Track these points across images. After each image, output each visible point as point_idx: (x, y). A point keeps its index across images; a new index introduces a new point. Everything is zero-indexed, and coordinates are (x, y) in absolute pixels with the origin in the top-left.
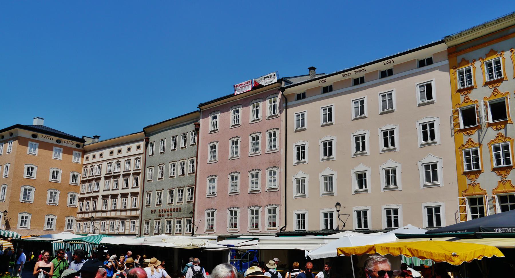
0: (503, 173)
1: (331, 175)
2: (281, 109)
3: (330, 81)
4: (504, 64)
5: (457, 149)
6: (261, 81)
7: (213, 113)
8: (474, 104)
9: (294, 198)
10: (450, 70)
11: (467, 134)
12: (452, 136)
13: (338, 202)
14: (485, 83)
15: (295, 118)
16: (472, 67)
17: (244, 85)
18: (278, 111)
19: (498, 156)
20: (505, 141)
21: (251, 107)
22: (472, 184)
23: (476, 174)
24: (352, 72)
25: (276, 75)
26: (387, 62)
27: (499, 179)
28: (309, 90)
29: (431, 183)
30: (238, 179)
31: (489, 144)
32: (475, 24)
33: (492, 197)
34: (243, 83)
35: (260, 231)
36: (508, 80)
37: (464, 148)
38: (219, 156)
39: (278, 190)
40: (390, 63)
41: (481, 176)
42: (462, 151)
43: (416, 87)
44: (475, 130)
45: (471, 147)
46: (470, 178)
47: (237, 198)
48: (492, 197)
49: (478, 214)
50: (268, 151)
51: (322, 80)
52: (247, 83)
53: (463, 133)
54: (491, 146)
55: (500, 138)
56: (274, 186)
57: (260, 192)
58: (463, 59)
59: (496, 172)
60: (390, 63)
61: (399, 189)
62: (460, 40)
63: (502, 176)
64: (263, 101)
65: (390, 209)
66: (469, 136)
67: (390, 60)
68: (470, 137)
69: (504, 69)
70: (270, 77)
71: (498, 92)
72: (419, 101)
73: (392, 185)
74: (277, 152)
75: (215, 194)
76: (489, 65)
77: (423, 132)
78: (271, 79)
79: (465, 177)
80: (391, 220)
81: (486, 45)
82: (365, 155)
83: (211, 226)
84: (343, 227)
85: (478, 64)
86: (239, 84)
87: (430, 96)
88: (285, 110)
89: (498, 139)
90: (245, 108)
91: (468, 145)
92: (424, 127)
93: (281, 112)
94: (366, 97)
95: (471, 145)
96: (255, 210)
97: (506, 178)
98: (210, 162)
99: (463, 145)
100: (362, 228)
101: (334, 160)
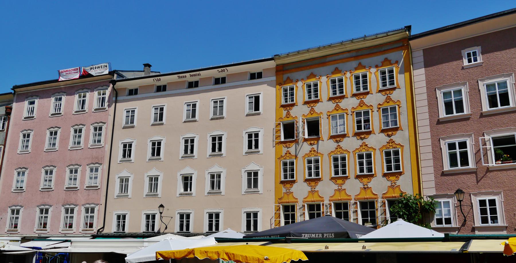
0: (313, 184)
2: (110, 103)
3: (164, 80)
4: (320, 87)
5: (277, 159)
7: (30, 98)
9: (115, 197)
11: (286, 146)
12: (273, 147)
13: (162, 204)
15: (125, 114)
16: (295, 86)
17: (70, 72)
18: (106, 104)
20: (368, 150)
21: (77, 96)
22: (287, 192)
23: (291, 184)
24: (188, 75)
27: (309, 189)
32: (321, 44)
33: (303, 205)
34: (70, 69)
35: (74, 232)
36: (322, 102)
37: (283, 159)
38: (32, 146)
40: (224, 72)
41: (295, 185)
45: (289, 159)
49: (289, 220)
50: (91, 146)
51: (156, 78)
52: (75, 70)
56: (94, 184)
58: (288, 78)
59: (308, 182)
60: (224, 72)
64: (90, 92)
66: (288, 148)
67: (224, 68)
68: (289, 149)
69: (320, 92)
70: (101, 68)
72: (247, 111)
74: (101, 148)
75: (23, 189)
79: (282, 185)
81: (308, 68)
82: (193, 158)
83: (89, 224)
84: (165, 230)
86: (65, 70)
88: (114, 104)
90: (69, 97)
93: (109, 106)
94: (199, 101)
95: (288, 156)
97: (315, 189)
98: (20, 152)
99: (282, 156)
100: (184, 231)
101: (161, 160)
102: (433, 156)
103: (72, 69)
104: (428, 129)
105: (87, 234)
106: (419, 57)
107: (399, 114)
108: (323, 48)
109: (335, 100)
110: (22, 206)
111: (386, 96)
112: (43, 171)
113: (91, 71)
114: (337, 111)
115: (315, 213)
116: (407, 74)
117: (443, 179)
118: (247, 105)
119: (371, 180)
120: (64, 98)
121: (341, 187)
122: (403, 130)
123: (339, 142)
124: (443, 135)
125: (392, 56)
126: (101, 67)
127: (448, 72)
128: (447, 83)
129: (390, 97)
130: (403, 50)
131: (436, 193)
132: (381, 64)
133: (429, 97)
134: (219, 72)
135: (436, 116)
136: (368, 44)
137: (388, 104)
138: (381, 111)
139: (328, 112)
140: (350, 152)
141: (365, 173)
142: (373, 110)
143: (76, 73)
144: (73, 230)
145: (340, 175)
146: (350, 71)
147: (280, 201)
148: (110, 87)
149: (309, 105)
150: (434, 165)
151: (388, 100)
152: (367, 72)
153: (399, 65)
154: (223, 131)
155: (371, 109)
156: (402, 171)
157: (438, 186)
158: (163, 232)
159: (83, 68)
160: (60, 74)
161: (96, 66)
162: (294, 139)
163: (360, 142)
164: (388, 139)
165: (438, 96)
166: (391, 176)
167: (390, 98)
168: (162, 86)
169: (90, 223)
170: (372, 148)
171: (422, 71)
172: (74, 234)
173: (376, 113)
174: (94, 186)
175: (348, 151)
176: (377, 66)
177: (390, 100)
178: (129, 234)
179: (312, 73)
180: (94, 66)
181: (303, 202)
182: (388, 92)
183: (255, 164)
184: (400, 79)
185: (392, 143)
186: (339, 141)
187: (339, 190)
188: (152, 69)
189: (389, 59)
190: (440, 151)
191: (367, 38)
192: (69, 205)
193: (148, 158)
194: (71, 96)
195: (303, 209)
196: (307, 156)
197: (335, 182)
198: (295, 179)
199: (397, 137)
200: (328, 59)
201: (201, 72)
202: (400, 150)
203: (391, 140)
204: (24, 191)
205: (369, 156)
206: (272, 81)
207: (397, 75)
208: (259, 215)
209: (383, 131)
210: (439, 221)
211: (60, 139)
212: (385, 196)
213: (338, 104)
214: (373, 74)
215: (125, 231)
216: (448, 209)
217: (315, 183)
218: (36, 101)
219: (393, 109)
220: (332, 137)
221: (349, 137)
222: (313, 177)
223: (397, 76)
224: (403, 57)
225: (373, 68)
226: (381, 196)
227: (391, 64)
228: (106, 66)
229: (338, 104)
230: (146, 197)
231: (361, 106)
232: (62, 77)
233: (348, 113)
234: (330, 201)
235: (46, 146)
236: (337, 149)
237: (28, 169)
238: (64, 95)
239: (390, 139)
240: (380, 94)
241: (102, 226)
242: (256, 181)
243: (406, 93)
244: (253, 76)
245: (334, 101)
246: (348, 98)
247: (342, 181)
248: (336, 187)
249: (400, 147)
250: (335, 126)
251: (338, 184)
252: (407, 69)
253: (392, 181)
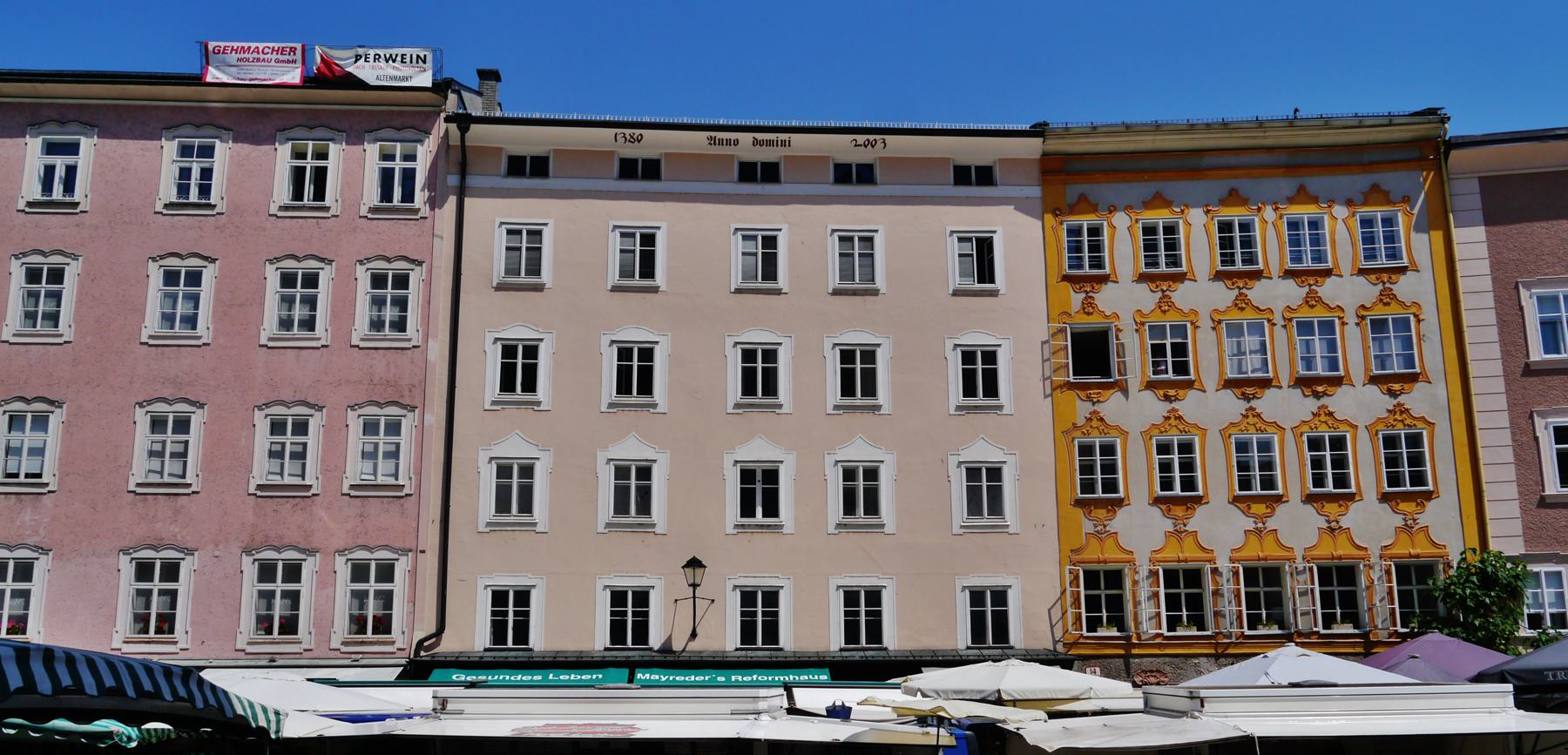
0: (1179, 511)
1: (647, 460)
2: (435, 190)
3: (654, 143)
4: (1188, 238)
5: (1058, 433)
6: (356, 62)
7: (53, 127)
8: (1107, 321)
9: (482, 528)
10: (1045, 216)
11: (1089, 398)
12: (1046, 397)
14: (1140, 274)
15: (501, 240)
16: (1105, 223)
17: (261, 56)
18: (420, 196)
19: (1317, 463)
20: (1335, 428)
21: (284, 151)
22: (1098, 532)
23: (1110, 508)
24: (746, 138)
25: (429, 58)
26: (866, 143)
27: (1168, 525)
28: (1008, 163)
29: (512, 518)
30: (402, 433)
31: (1146, 435)
32: (1163, 117)
33: (1150, 571)
34: (261, 46)
35: (305, 650)
36: (1196, 281)
37: (1078, 433)
38: (79, 319)
39: (407, 495)
40: (873, 146)
41: (1122, 513)
42: (1073, 441)
43: (948, 238)
44: (1109, 389)
45: (1255, 432)
46: (1251, 511)
47: (182, 506)
48: (1150, 571)
49: (1101, 612)
50: (362, 340)
51: (628, 132)
52: (282, 51)
53: (1078, 395)
54: (1151, 439)
55: (1172, 421)
56: (384, 478)
57: (314, 495)
58: (1083, 198)
59: (1163, 507)
60: (873, 146)
61: (886, 530)
62: (1082, 144)
63: (1405, 515)
64: (98, 137)
65: (859, 589)
66: (1094, 404)
67: (878, 137)
68: (1097, 407)
69: (1188, 250)
70: (402, 62)
71: (1172, 305)
72: (955, 280)
73: (633, 517)
74: (409, 349)
75: (44, 480)
76: (1149, 230)
77: (744, 369)
78: (406, 71)
79: (1079, 512)
80: (858, 623)
81: (1146, 177)
82: (778, 411)
83: (374, 621)
84: (689, 640)
85: (1121, 220)
86: (236, 45)
87: (986, 271)
88: (452, 201)
89: (1170, 425)
90: (246, 148)
91: (1091, 427)
92: (509, 351)
93: (434, 203)
94: (785, 227)
95: (1097, 428)
96: (373, 565)
97: (1185, 525)
98: (14, 335)
101: (658, 410)
102: (1516, 455)
103: (271, 45)
104: (1500, 385)
105: (366, 656)
106: (1467, 194)
107: (1419, 340)
108: (1204, 127)
109: (1234, 280)
110: (42, 549)
111: (1380, 287)
112: (142, 419)
113: (358, 68)
114: (1239, 311)
115: (1100, 596)
116: (1438, 236)
117: (1543, 515)
118: (954, 264)
119: (1347, 508)
120: (224, 151)
121: (1264, 524)
122: (1430, 383)
123: (1253, 399)
124: (1541, 404)
125: (1393, 180)
126: (402, 58)
127: (1548, 247)
128: (1547, 274)
129: (1392, 290)
130: (1423, 170)
131: (1527, 551)
132: (1359, 198)
133: (1500, 302)
134: (856, 146)
135: (1519, 355)
136: (1327, 137)
137: (1386, 310)
138: (1367, 324)
139: (1216, 311)
140: (1284, 429)
141: (1330, 487)
142: (1345, 320)
143: (286, 65)
144: (301, 642)
145: (1257, 490)
146: (1275, 203)
147: (1075, 557)
148: (431, 136)
149: (1154, 285)
150: (1517, 478)
151: (1387, 297)
152: (1326, 213)
153: (1412, 208)
154: (877, 335)
155: (1340, 318)
156: (1432, 489)
157: (1529, 535)
158: (683, 651)
159: (318, 50)
160: (206, 57)
161: (378, 52)
162: (1112, 380)
163: (1312, 404)
164: (1390, 403)
165: (1523, 303)
166: (1402, 502)
167: (1393, 294)
168: (759, 165)
169: (374, 617)
170: (1346, 422)
171: (1479, 232)
172: (306, 654)
173: (1353, 332)
174: (384, 483)
175: (1277, 425)
176: (1349, 203)
177: (1316, 301)
178: (544, 654)
179: (1157, 192)
180: (372, 52)
181: (1232, 560)
182: (1385, 277)
183: (530, 441)
184: (1420, 246)
185: (1402, 413)
186: (1251, 396)
187: (1258, 532)
188: (501, 90)
189: (1384, 187)
190: (1532, 442)
191: (1299, 124)
192: (278, 549)
193: (488, 399)
194: (260, 147)
195: (1153, 582)
196: (1157, 431)
197: (1245, 510)
198: (1123, 496)
199: (1417, 400)
200: (1208, 161)
201: (795, 137)
202: (1425, 433)
203: (1399, 405)
204: (50, 488)
205: (1338, 443)
206: (1027, 198)
207: (1410, 233)
208: (535, 598)
209: (1374, 380)
210: (1535, 621)
211: (218, 300)
212: (1388, 552)
213: (1242, 291)
214: (1340, 221)
215: (531, 646)
216: (1556, 592)
217: (1187, 511)
218: (86, 144)
219: (1403, 324)
220: (1229, 384)
221: (1280, 387)
222: (1330, 487)
223: (1410, 238)
224: (1424, 188)
225: (1340, 204)
226: (1378, 552)
227: (1393, 203)
228: (422, 57)
229: (1244, 291)
230: (606, 531)
231: (1309, 306)
232: (217, 68)
233: (1274, 321)
234: (1233, 563)
235: (152, 323)
236: (1248, 417)
237: (65, 406)
238: (225, 137)
239: (1395, 402)
240: (1361, 279)
241: (433, 630)
242: (996, 495)
243: (1437, 285)
244: (963, 175)
245: (1154, 285)
246: (1271, 278)
247: (1267, 507)
248: (1249, 524)
249: (1424, 426)
250: (1235, 352)
251: (1255, 516)
252: (1438, 219)
253: (1405, 515)
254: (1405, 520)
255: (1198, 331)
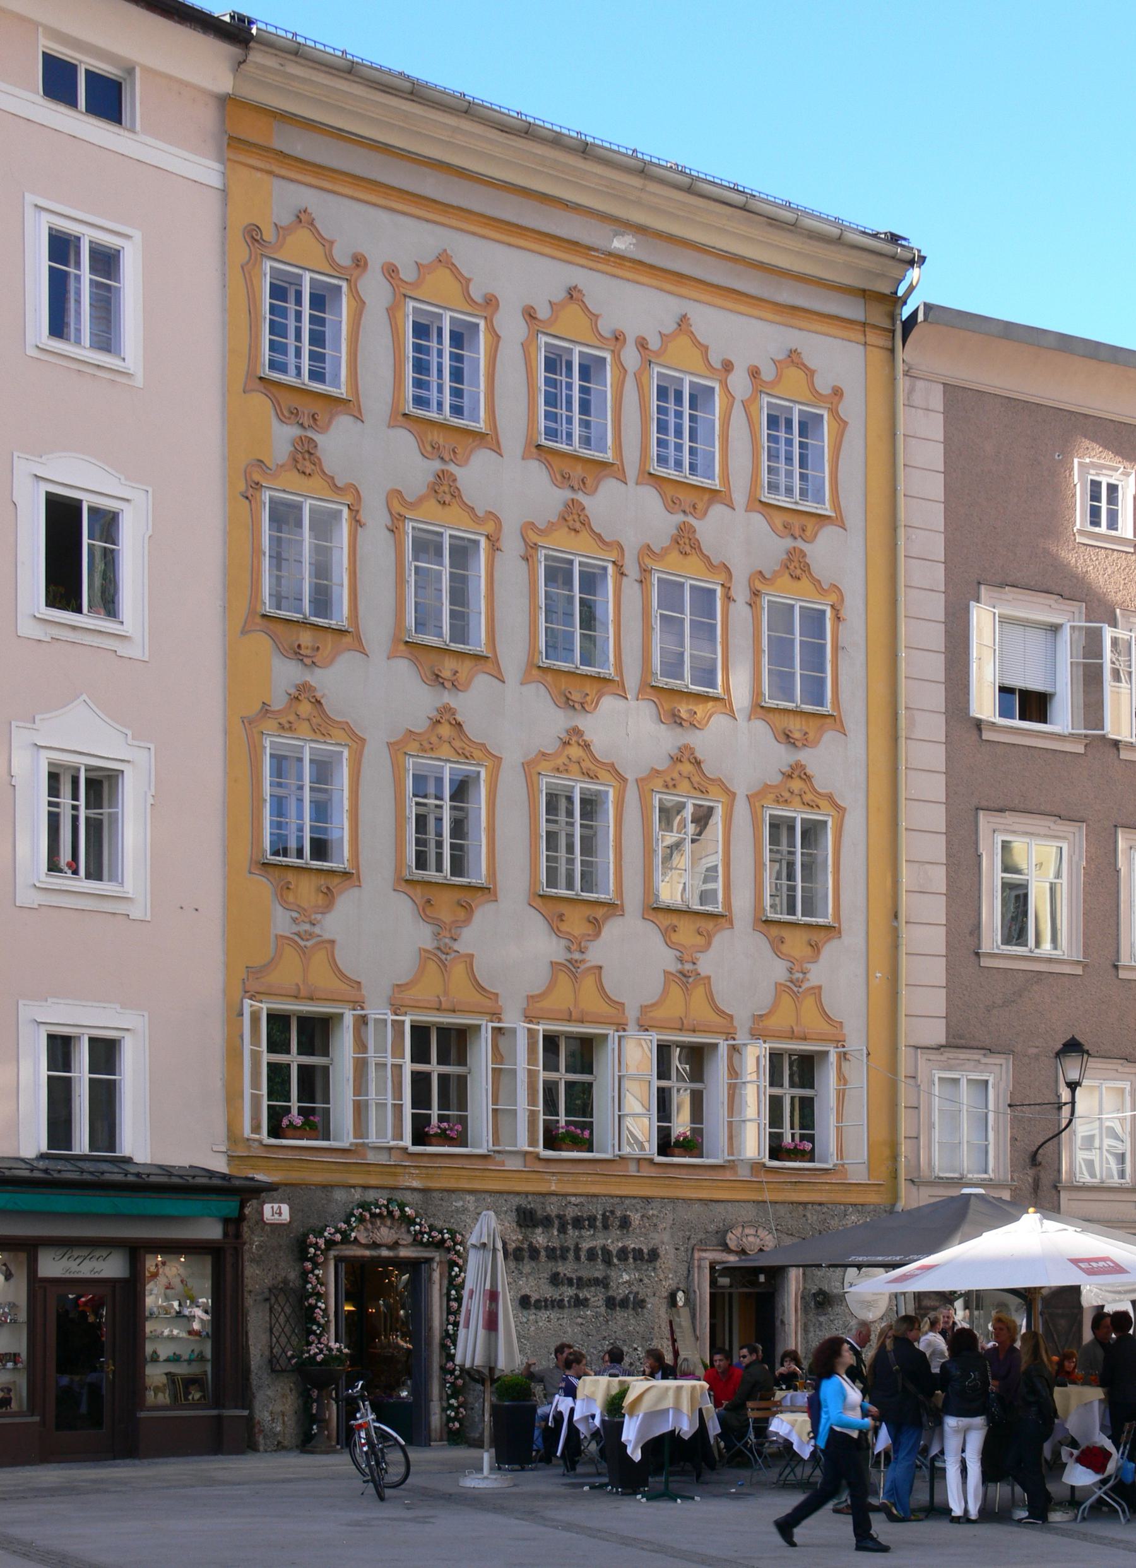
13: (1073, 1038)
31: (529, 768)
99: (266, 710)
100: (76, 1151)
173: (740, 610)
254: (790, 971)
255: (732, 605)
